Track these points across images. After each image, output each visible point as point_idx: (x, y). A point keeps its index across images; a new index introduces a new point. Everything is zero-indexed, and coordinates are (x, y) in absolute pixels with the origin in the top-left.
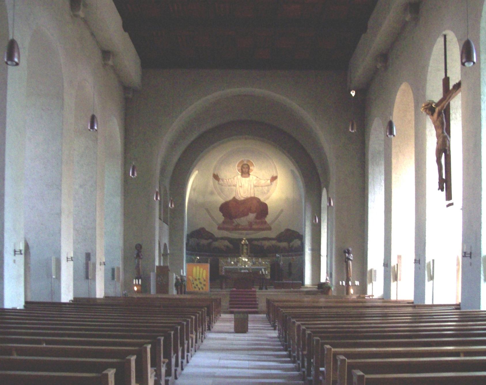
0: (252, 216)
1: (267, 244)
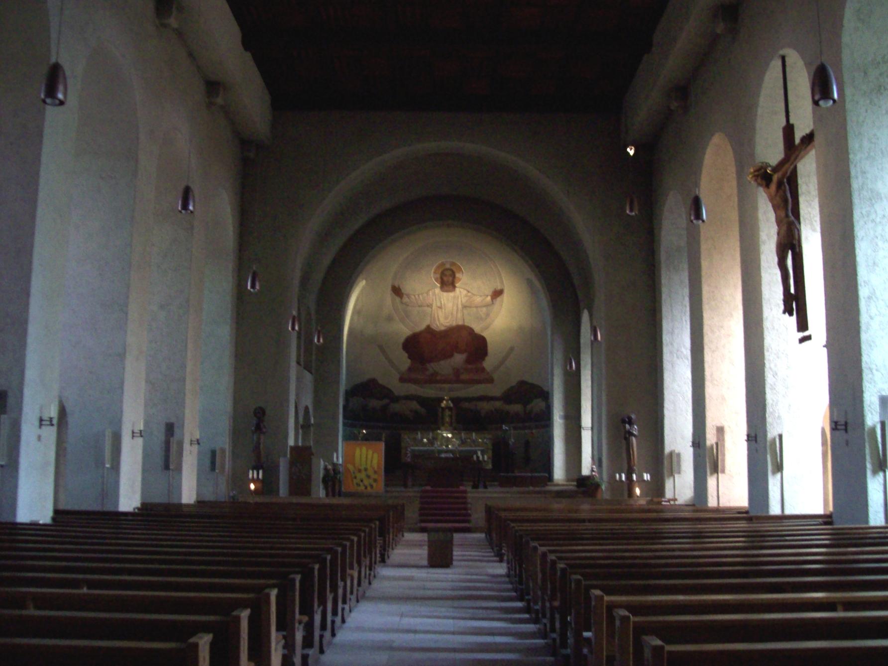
0: (459, 359)
1: (485, 406)
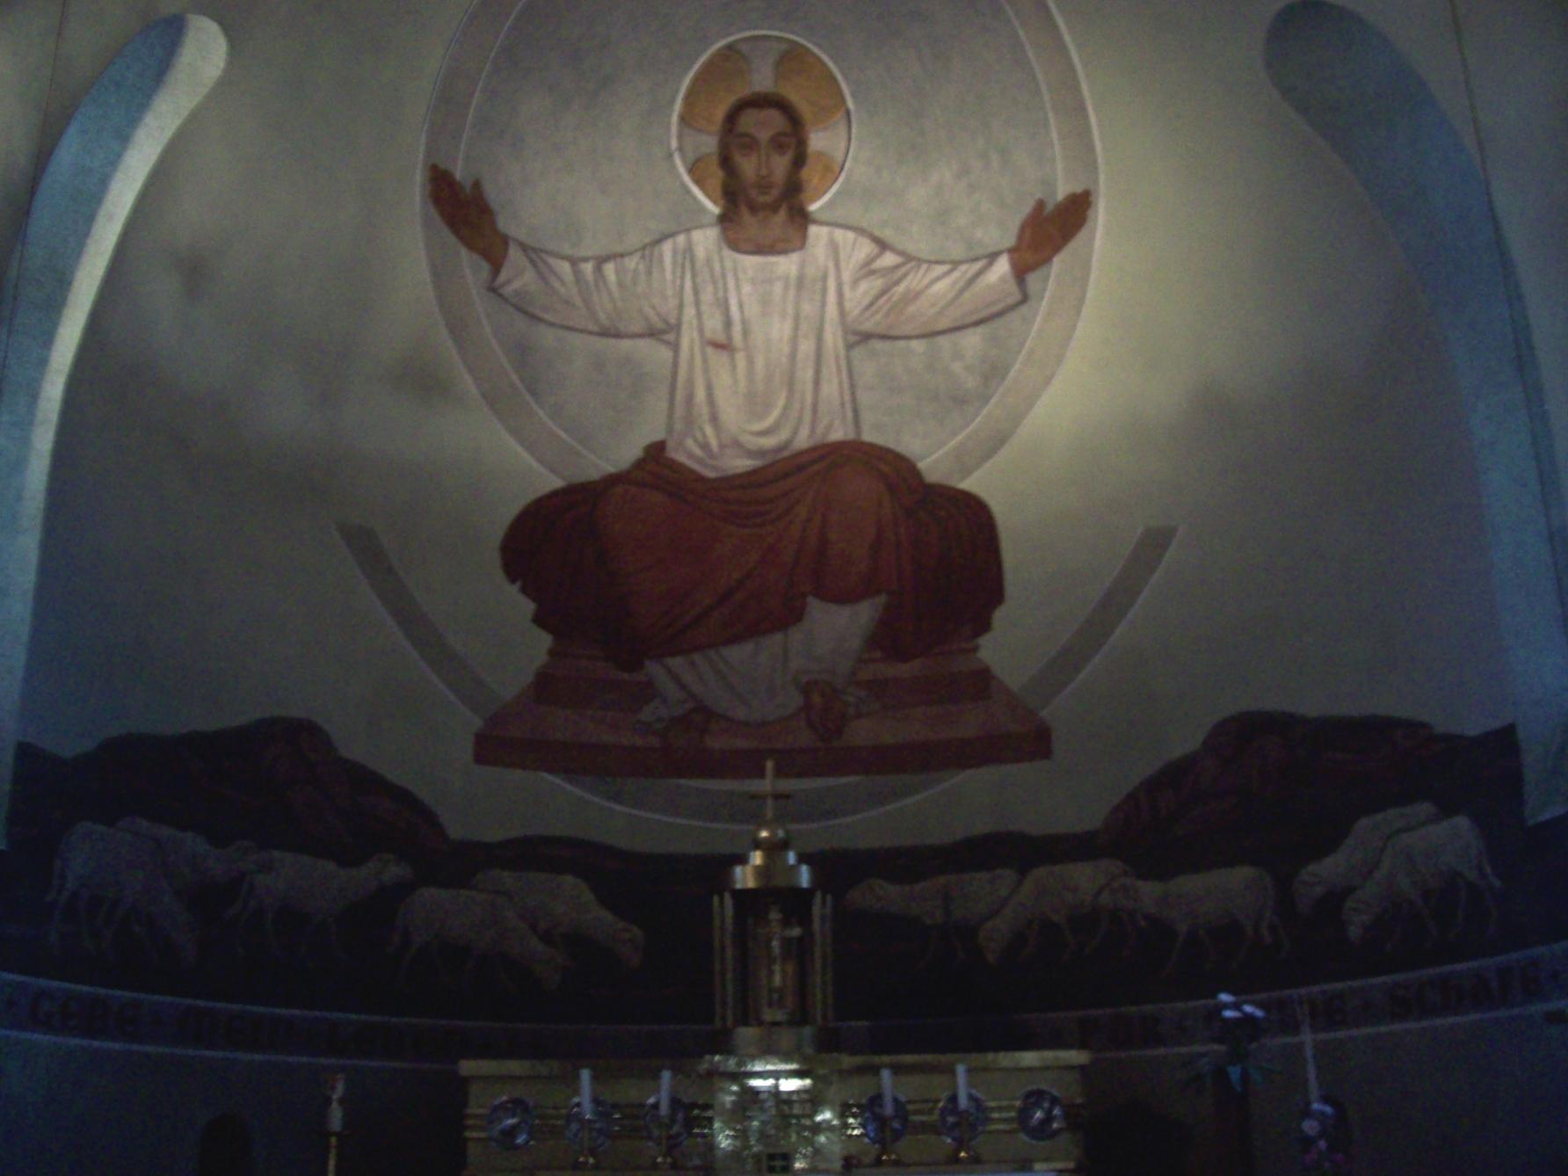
0: (836, 629)
1: (999, 903)
